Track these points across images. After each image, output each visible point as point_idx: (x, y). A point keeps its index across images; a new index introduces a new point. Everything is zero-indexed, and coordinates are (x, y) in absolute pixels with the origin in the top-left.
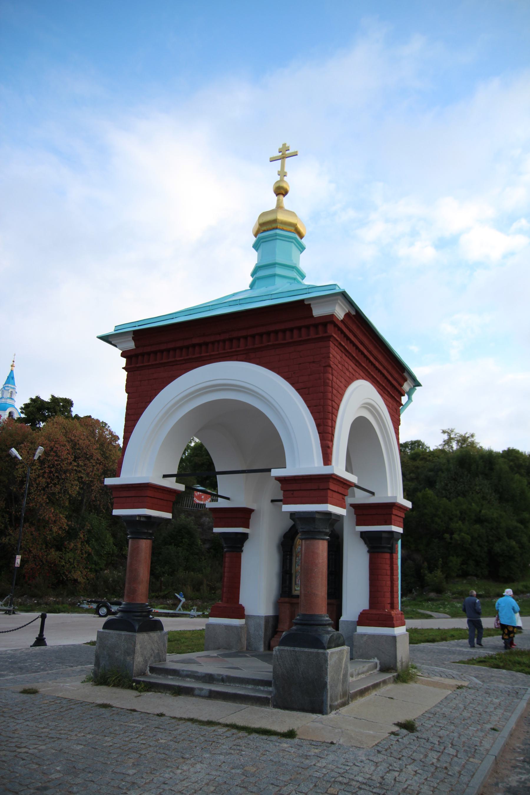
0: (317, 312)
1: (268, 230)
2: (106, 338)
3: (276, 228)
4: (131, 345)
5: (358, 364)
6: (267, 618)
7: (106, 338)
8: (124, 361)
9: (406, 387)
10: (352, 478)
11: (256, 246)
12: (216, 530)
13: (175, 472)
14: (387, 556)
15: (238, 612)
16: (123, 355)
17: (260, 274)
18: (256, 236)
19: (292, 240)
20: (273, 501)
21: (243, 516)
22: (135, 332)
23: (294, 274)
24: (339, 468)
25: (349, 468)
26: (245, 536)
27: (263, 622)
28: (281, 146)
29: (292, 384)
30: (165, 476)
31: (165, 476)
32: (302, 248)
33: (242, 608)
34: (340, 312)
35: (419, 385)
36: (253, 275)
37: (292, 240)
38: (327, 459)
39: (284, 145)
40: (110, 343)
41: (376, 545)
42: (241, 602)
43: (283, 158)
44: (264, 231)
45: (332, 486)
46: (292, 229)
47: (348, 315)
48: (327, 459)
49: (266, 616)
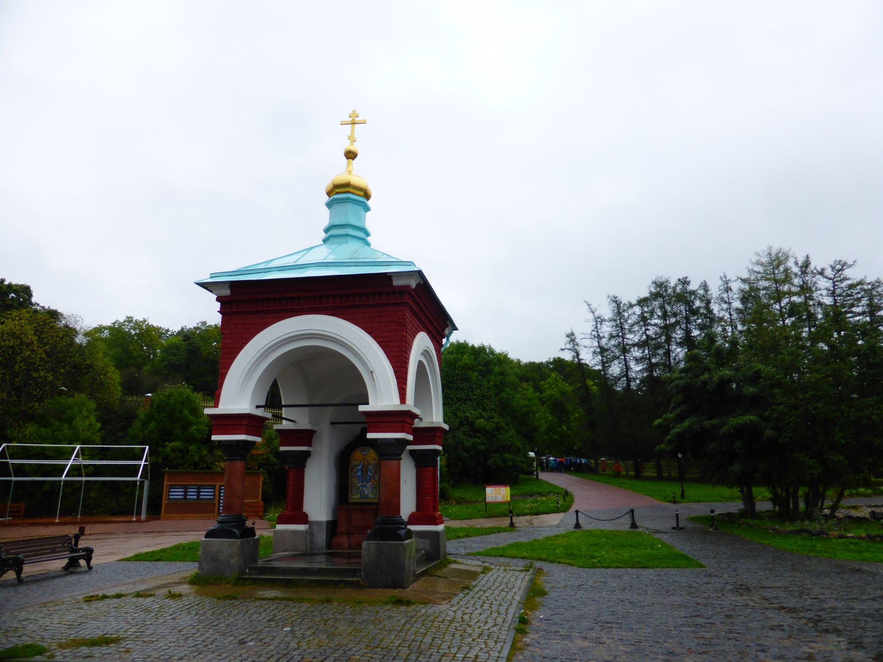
0: (396, 282)
1: (341, 193)
2: (205, 285)
3: (349, 192)
4: (227, 292)
5: (419, 319)
6: (328, 522)
7: (205, 285)
8: (218, 305)
9: (447, 331)
10: (416, 411)
11: (329, 205)
12: (282, 449)
13: (264, 404)
14: (431, 469)
15: (303, 518)
16: (218, 300)
17: (334, 232)
18: (329, 194)
19: (347, 189)
20: (332, 423)
21: (306, 436)
22: (233, 285)
23: (361, 234)
24: (410, 404)
25: (415, 405)
26: (307, 454)
27: (325, 527)
28: (351, 112)
29: (375, 338)
30: (257, 407)
31: (257, 407)
32: (367, 209)
33: (306, 516)
34: (413, 284)
35: (456, 329)
36: (326, 231)
37: (347, 189)
38: (403, 400)
39: (354, 111)
40: (206, 288)
41: (422, 461)
42: (304, 510)
43: (353, 123)
44: (337, 193)
45: (439, 434)
46: (362, 193)
47: (418, 285)
48: (403, 400)
49: (159, 519)
